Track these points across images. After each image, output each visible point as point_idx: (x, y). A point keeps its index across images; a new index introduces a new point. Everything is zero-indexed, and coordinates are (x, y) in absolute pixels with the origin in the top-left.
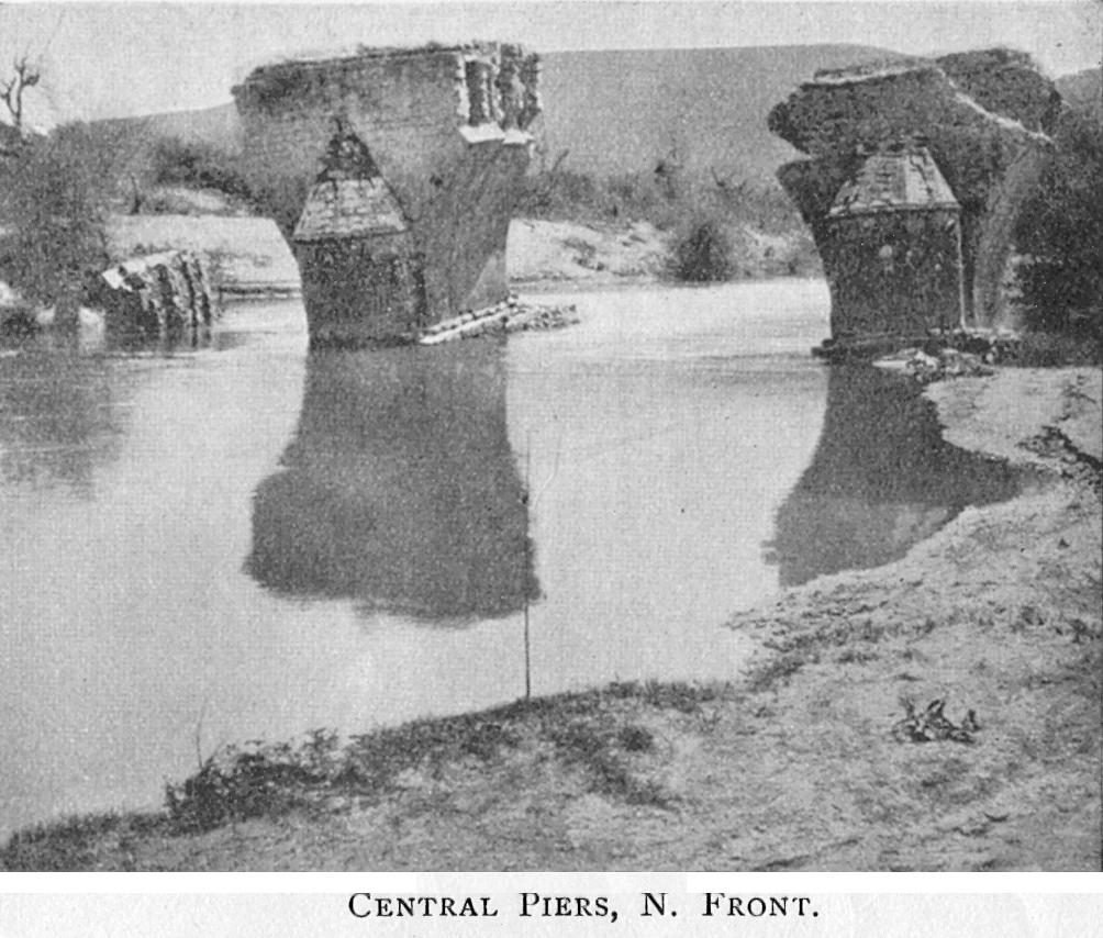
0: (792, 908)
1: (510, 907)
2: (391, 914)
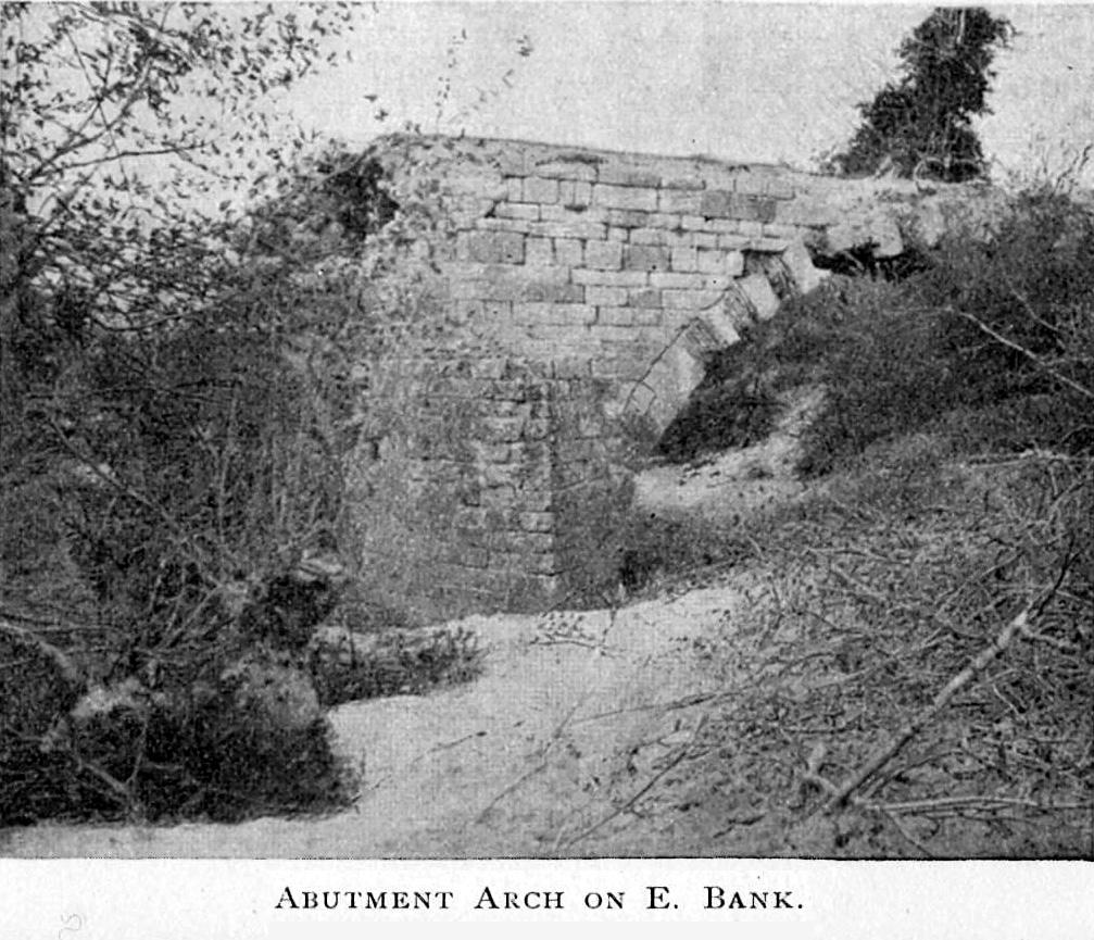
0: (435, 902)
1: (637, 899)
2: (407, 906)
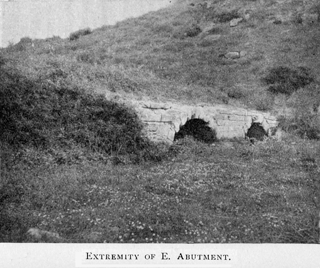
0: (223, 258)
1: (159, 257)
2: (215, 259)
